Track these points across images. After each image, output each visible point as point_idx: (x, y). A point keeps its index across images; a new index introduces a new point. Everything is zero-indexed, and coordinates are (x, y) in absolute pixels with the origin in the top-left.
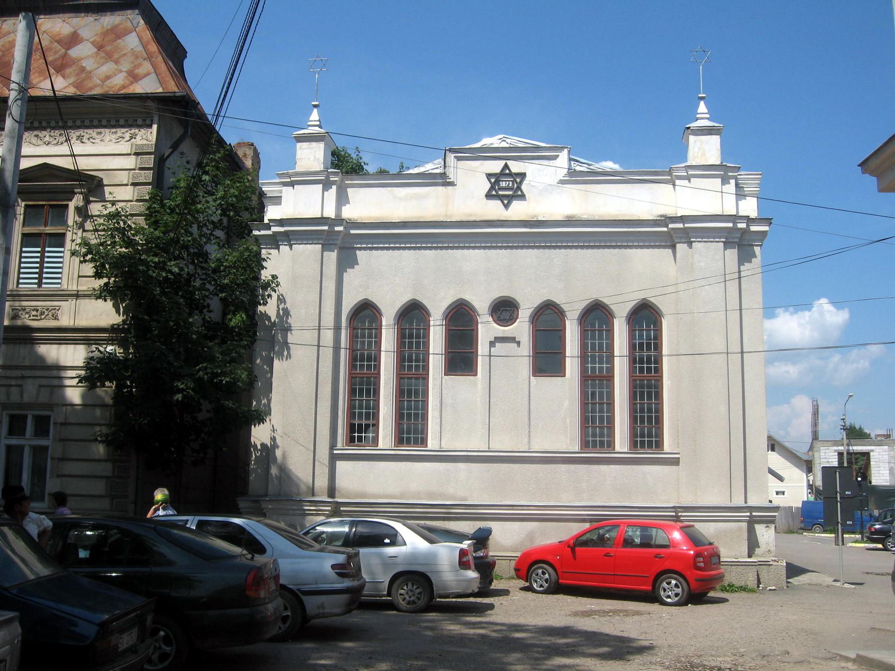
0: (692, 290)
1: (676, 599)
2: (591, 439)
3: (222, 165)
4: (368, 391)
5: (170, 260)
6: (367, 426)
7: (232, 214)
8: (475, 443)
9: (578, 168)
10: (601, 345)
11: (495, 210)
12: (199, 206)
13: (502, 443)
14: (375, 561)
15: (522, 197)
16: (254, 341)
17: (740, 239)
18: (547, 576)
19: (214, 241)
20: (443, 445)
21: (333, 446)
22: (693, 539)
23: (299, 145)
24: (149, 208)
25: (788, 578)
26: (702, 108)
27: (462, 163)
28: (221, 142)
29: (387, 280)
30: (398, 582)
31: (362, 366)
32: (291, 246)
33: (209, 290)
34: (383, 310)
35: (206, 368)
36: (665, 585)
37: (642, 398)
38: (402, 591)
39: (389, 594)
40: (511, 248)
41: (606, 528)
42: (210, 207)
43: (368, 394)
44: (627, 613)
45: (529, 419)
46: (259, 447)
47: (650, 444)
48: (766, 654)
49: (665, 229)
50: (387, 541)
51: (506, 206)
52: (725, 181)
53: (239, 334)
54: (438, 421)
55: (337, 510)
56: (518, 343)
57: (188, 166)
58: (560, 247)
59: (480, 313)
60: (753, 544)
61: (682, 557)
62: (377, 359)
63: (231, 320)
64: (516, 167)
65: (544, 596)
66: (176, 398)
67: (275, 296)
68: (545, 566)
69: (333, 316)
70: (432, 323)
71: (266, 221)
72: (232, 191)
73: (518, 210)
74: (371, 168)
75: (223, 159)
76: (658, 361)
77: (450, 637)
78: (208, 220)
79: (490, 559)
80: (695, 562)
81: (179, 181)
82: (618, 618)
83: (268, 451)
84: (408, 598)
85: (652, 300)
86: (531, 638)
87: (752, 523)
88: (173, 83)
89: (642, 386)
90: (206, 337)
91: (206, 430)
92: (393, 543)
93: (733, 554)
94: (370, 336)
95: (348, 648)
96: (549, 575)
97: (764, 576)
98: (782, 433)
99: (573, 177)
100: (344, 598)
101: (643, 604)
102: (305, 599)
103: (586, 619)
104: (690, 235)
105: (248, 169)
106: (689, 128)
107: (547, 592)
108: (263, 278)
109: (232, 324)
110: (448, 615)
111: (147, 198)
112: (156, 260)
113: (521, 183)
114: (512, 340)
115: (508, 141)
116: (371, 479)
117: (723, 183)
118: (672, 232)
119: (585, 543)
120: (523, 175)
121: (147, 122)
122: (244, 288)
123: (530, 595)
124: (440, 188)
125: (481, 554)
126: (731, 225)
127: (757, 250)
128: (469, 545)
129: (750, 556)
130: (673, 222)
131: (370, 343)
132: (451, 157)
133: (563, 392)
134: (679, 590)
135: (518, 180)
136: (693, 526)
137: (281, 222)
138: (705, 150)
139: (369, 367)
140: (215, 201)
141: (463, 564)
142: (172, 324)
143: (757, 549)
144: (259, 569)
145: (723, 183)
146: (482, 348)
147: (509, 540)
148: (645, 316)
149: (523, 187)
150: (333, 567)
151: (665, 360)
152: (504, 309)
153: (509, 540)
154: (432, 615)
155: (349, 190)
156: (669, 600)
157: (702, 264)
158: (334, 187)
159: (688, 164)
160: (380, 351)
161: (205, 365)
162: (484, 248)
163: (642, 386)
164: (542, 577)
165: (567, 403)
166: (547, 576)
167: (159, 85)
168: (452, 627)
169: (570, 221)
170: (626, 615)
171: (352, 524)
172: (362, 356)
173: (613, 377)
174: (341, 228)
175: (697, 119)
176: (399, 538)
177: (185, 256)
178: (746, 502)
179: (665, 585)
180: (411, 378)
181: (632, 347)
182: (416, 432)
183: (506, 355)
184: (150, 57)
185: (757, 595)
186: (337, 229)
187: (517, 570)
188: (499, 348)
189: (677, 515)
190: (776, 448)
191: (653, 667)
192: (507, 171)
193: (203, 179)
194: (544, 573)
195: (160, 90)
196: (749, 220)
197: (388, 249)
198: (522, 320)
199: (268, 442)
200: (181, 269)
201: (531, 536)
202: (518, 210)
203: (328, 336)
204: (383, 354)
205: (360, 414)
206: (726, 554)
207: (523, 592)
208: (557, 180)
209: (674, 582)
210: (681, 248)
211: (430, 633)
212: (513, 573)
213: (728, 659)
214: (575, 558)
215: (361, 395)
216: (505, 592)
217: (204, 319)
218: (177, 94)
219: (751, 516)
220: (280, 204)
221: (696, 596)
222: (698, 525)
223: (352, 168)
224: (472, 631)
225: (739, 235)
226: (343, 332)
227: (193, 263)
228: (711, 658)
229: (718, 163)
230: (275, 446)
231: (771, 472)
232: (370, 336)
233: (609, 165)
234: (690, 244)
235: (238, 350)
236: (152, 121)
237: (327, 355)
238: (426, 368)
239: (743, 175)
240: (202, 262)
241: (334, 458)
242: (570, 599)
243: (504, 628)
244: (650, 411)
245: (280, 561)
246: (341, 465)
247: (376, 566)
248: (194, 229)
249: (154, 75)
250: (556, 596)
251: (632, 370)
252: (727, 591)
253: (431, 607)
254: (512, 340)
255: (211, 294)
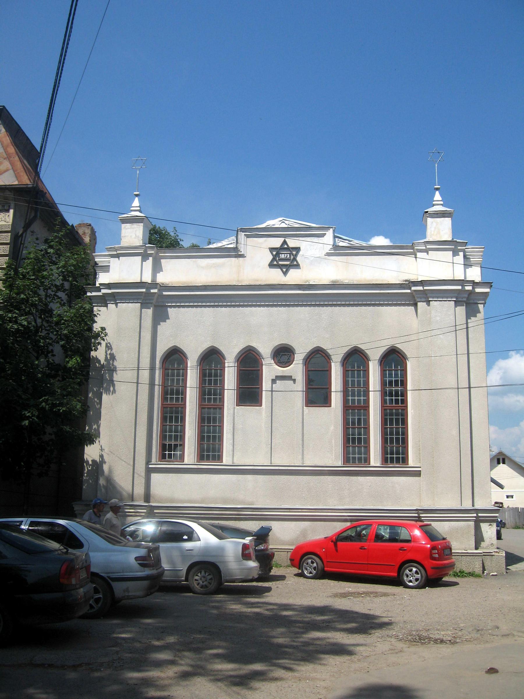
0: (432, 339)
1: (417, 583)
2: (351, 456)
3: (64, 241)
4: (177, 418)
5: (22, 315)
6: (176, 446)
7: (70, 279)
8: (260, 459)
9: (341, 244)
10: (359, 382)
11: (276, 276)
12: (45, 273)
13: (282, 460)
14: (176, 554)
15: (297, 266)
16: (87, 380)
17: (467, 299)
18: (315, 565)
19: (57, 301)
20: (235, 461)
21: (148, 461)
22: (430, 535)
23: (123, 226)
24: (5, 274)
25: (507, 566)
26: (437, 196)
27: (250, 240)
28: (64, 223)
29: (192, 331)
30: (193, 570)
31: (172, 399)
32: (116, 304)
33: (52, 339)
34: (189, 355)
35: (47, 400)
36: (407, 572)
37: (391, 424)
38: (196, 578)
39: (187, 580)
40: (289, 306)
41: (362, 527)
42: (54, 273)
43: (177, 421)
44: (376, 594)
45: (303, 441)
46: (90, 463)
47: (398, 459)
48: (481, 628)
49: (409, 291)
50: (185, 537)
51: (285, 273)
52: (455, 253)
53: (75, 373)
54: (231, 442)
55: (151, 512)
56: (294, 381)
57: (37, 242)
58: (327, 305)
59: (264, 357)
60: (479, 539)
61: (420, 550)
62: (184, 393)
63: (68, 362)
64: (292, 243)
65: (312, 580)
66: (23, 424)
67: (104, 344)
68: (313, 557)
69: (149, 359)
70: (226, 365)
71: (97, 285)
72: (72, 261)
73: (294, 277)
74: (186, 244)
75: (66, 235)
76: (404, 394)
77: (231, 615)
78: (52, 285)
79: (269, 552)
80: (431, 554)
81: (30, 253)
82: (368, 598)
83: (98, 466)
84: (201, 583)
85: (359, 346)
86: (295, 615)
87: (478, 522)
88: (26, 177)
89: (391, 414)
90: (49, 376)
91: (49, 448)
92: (190, 539)
93: (463, 547)
94: (178, 375)
95: (149, 624)
96: (317, 564)
97: (487, 564)
98: (514, 449)
99: (337, 251)
100: (146, 583)
101: (391, 587)
102: (114, 584)
103: (343, 599)
104: (428, 295)
105: (86, 245)
106: (427, 212)
107: (314, 578)
108: (95, 330)
109: (69, 365)
110: (233, 596)
111: (5, 266)
112: (10, 315)
113: (296, 255)
114: (289, 378)
115: (286, 222)
116: (174, 488)
117: (454, 255)
118: (414, 293)
119: (348, 538)
120: (298, 249)
121: (6, 208)
122: (80, 337)
123: (302, 579)
124: (233, 259)
125: (262, 547)
126: (460, 287)
127: (481, 307)
128: (251, 541)
129: (476, 548)
130: (415, 286)
131: (178, 380)
132: (242, 235)
133: (329, 419)
134: (419, 576)
135: (294, 253)
136: (430, 525)
137: (109, 286)
138: (440, 229)
139: (177, 399)
140: (58, 268)
141: (246, 556)
142: (22, 365)
143: (482, 543)
144: (72, 561)
145: (454, 255)
146: (266, 385)
147: (285, 536)
148: (394, 359)
149: (298, 259)
150: (137, 559)
151: (409, 393)
152: (283, 354)
153: (285, 536)
154: (220, 597)
155: (163, 261)
156: (411, 584)
157: (438, 318)
158: (151, 258)
159: (427, 240)
160: (186, 387)
161: (46, 398)
162: (268, 306)
163: (391, 414)
164: (311, 565)
165: (332, 428)
166: (315, 565)
167: (15, 179)
168: (234, 607)
169: (334, 285)
170: (375, 597)
171: (160, 523)
172: (172, 390)
173: (369, 407)
174: (155, 291)
175: (434, 205)
176: (195, 535)
177: (34, 312)
178: (473, 506)
179: (407, 572)
180: (210, 408)
181: (383, 384)
182: (214, 450)
183: (284, 388)
184: (9, 157)
185: (482, 579)
186: (152, 291)
187: (291, 560)
188: (279, 384)
189: (418, 517)
190: (506, 461)
191: (389, 639)
192: (286, 246)
193: (49, 251)
194: (312, 563)
195: (16, 183)
196: (474, 284)
197: (197, 306)
198: (297, 362)
199: (97, 459)
200: (29, 323)
201: (304, 533)
202: (294, 277)
203: (145, 375)
204: (188, 389)
205: (170, 436)
206: (457, 547)
207: (296, 578)
208: (324, 253)
209: (414, 569)
210: (421, 305)
211: (215, 612)
212: (289, 562)
213: (450, 633)
214: (337, 550)
215: (171, 421)
216: (282, 578)
217: (48, 361)
218: (29, 186)
219: (477, 517)
220: (108, 271)
221: (433, 580)
222: (434, 524)
223: (170, 243)
224: (249, 610)
225: (466, 296)
226: (157, 372)
227: (40, 317)
228: (436, 632)
229: (450, 239)
230: (103, 461)
231: (493, 481)
232: (178, 375)
233: (379, 241)
234: (428, 303)
235: (72, 386)
236: (9, 206)
237: (144, 390)
238: (222, 400)
239: (469, 249)
240: (47, 317)
241: (149, 471)
242: (332, 583)
243: (275, 607)
244: (397, 433)
245: (91, 554)
246: (154, 477)
247: (173, 560)
248: (42, 293)
249: (11, 172)
250: (322, 581)
251: (383, 402)
252: (459, 576)
253: (221, 589)
254: (289, 378)
255: (54, 342)
